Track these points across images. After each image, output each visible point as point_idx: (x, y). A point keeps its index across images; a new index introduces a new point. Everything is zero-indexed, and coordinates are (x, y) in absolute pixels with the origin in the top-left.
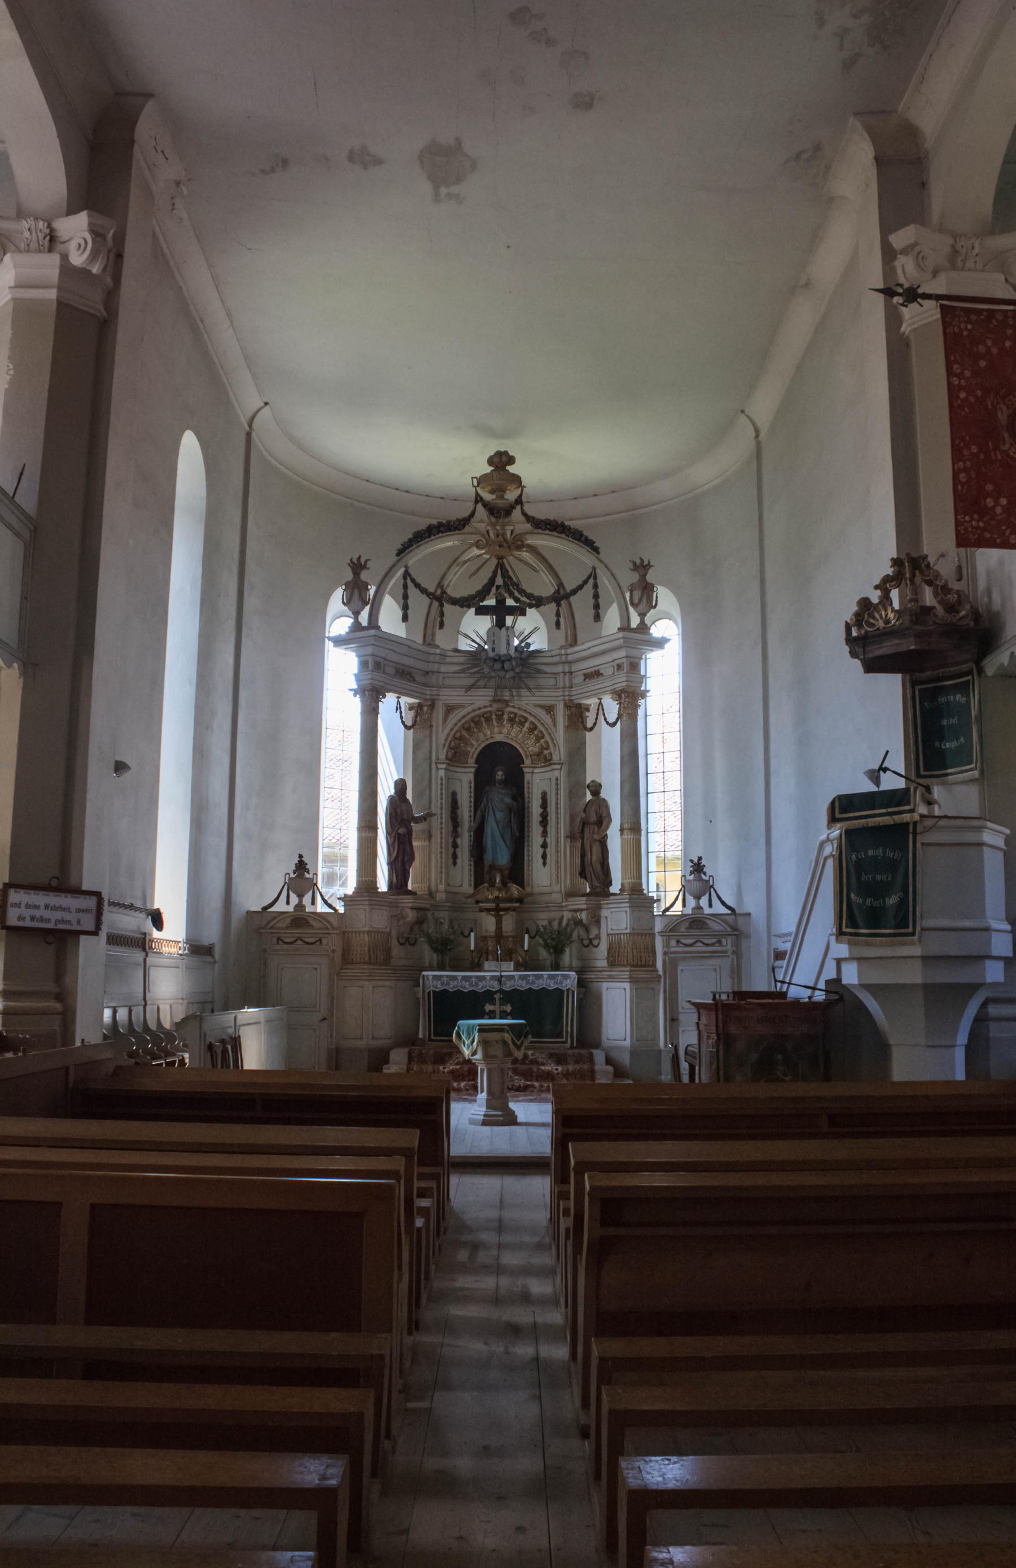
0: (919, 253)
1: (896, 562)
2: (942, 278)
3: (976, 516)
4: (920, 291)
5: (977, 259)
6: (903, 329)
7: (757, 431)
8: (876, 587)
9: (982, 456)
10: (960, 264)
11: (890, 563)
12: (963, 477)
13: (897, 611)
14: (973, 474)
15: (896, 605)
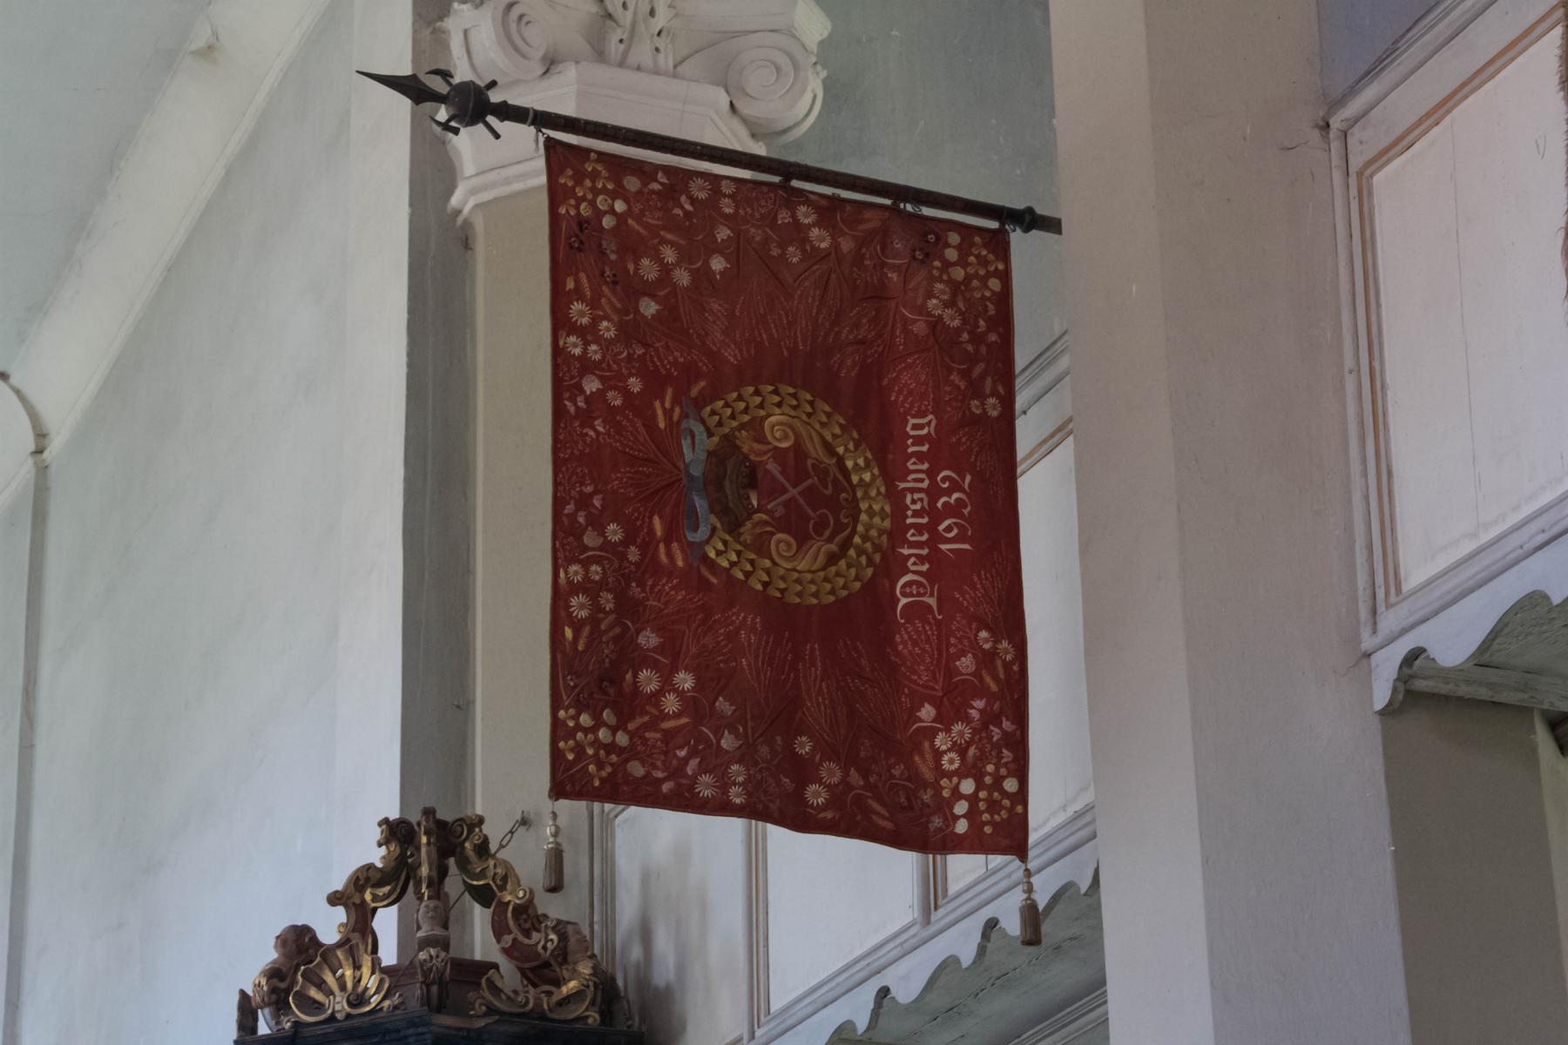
0: (521, 17)
1: (397, 832)
2: (569, 75)
3: (607, 715)
4: (495, 97)
5: (661, 42)
6: (455, 200)
7: (41, 436)
8: (334, 899)
9: (633, 554)
10: (614, 49)
11: (377, 833)
12: (579, 606)
13: (388, 971)
14: (607, 600)
15: (389, 954)
